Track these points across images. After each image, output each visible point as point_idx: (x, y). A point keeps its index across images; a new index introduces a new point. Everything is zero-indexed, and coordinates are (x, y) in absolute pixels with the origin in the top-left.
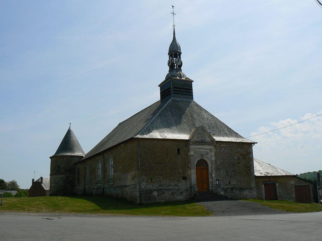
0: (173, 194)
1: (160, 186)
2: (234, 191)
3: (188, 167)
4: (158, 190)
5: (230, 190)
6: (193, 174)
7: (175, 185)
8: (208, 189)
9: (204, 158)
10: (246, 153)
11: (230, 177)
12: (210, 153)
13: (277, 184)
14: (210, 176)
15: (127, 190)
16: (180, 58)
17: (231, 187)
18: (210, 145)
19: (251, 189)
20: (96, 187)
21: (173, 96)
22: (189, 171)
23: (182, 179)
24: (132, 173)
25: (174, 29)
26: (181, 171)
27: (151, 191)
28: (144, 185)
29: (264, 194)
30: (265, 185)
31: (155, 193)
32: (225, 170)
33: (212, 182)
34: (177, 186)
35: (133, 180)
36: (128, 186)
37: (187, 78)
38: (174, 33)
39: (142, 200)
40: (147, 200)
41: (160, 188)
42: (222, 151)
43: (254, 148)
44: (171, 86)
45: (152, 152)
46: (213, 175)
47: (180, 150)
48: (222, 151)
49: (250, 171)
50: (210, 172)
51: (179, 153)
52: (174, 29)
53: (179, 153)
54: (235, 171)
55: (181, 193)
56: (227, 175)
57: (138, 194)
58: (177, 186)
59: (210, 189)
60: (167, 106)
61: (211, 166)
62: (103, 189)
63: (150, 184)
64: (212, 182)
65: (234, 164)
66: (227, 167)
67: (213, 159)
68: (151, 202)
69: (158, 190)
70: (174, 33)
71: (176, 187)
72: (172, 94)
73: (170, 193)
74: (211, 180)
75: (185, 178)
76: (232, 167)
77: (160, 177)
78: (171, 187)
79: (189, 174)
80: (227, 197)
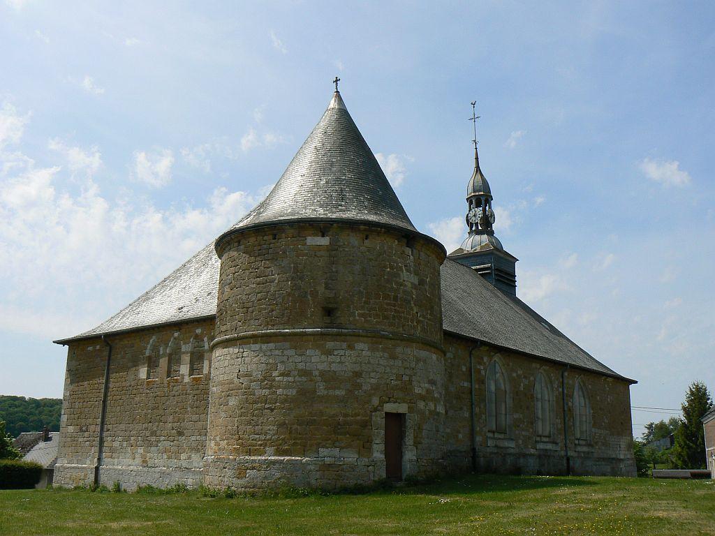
20: (532, 451)
38: (477, 158)
62: (568, 459)
70: (477, 158)
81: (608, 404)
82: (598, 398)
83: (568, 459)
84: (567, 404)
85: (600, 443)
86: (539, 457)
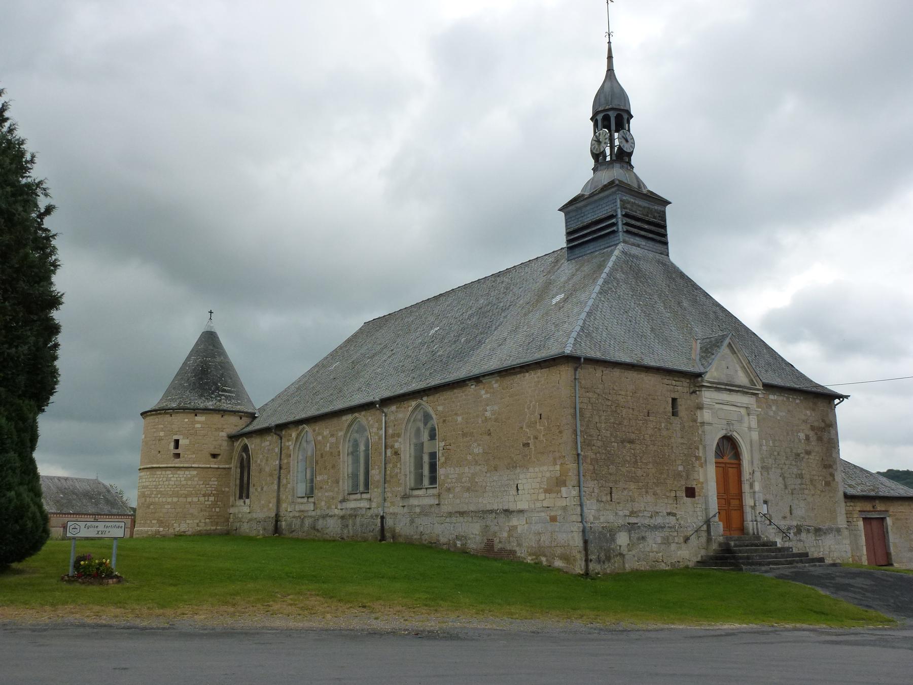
0: (666, 542)
1: (633, 513)
2: (804, 535)
3: (698, 458)
4: (631, 528)
5: (795, 534)
6: (708, 477)
7: (669, 514)
8: (742, 529)
9: (735, 434)
10: (823, 425)
11: (792, 494)
12: (746, 418)
13: (889, 521)
14: (746, 487)
15: (516, 527)
16: (629, 130)
17: (795, 523)
18: (747, 393)
19: (838, 530)
20: (336, 512)
21: (624, 242)
22: (701, 470)
23: (684, 495)
24: (545, 471)
25: (609, 43)
26: (680, 468)
27: (610, 534)
28: (600, 515)
29: (865, 548)
30: (864, 519)
31: (622, 539)
32: (779, 471)
33: (754, 507)
34: (674, 515)
35: (546, 491)
36: (521, 511)
37: (649, 191)
38: (610, 57)
39: (591, 560)
40: (604, 562)
41: (633, 520)
42: (771, 413)
43: (842, 411)
44: (616, 211)
45: (609, 403)
46: (757, 487)
47: (679, 402)
48: (771, 413)
49: (834, 480)
50: (746, 476)
51: (675, 414)
52: (609, 43)
53: (675, 414)
54: (801, 476)
55: (686, 540)
56: (786, 487)
57: (578, 542)
58: (674, 515)
59: (751, 528)
60: (613, 269)
61: (750, 458)
62: (382, 518)
63: (608, 507)
64: (754, 507)
65: (798, 455)
66: (785, 464)
67: (755, 436)
68: (177, 529)
69: (631, 528)
70: (610, 57)
71: (672, 520)
72: (621, 234)
73: (659, 540)
74: (748, 501)
75: (691, 493)
76: (794, 463)
77: (632, 486)
78: (659, 520)
79: (701, 480)
80: (821, 560)
81: (486, 420)
82: (460, 419)
83: (382, 518)
84: (392, 447)
85: (457, 490)
86: (343, 517)
